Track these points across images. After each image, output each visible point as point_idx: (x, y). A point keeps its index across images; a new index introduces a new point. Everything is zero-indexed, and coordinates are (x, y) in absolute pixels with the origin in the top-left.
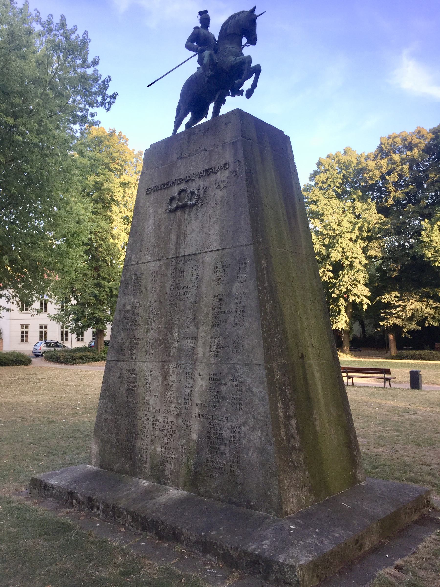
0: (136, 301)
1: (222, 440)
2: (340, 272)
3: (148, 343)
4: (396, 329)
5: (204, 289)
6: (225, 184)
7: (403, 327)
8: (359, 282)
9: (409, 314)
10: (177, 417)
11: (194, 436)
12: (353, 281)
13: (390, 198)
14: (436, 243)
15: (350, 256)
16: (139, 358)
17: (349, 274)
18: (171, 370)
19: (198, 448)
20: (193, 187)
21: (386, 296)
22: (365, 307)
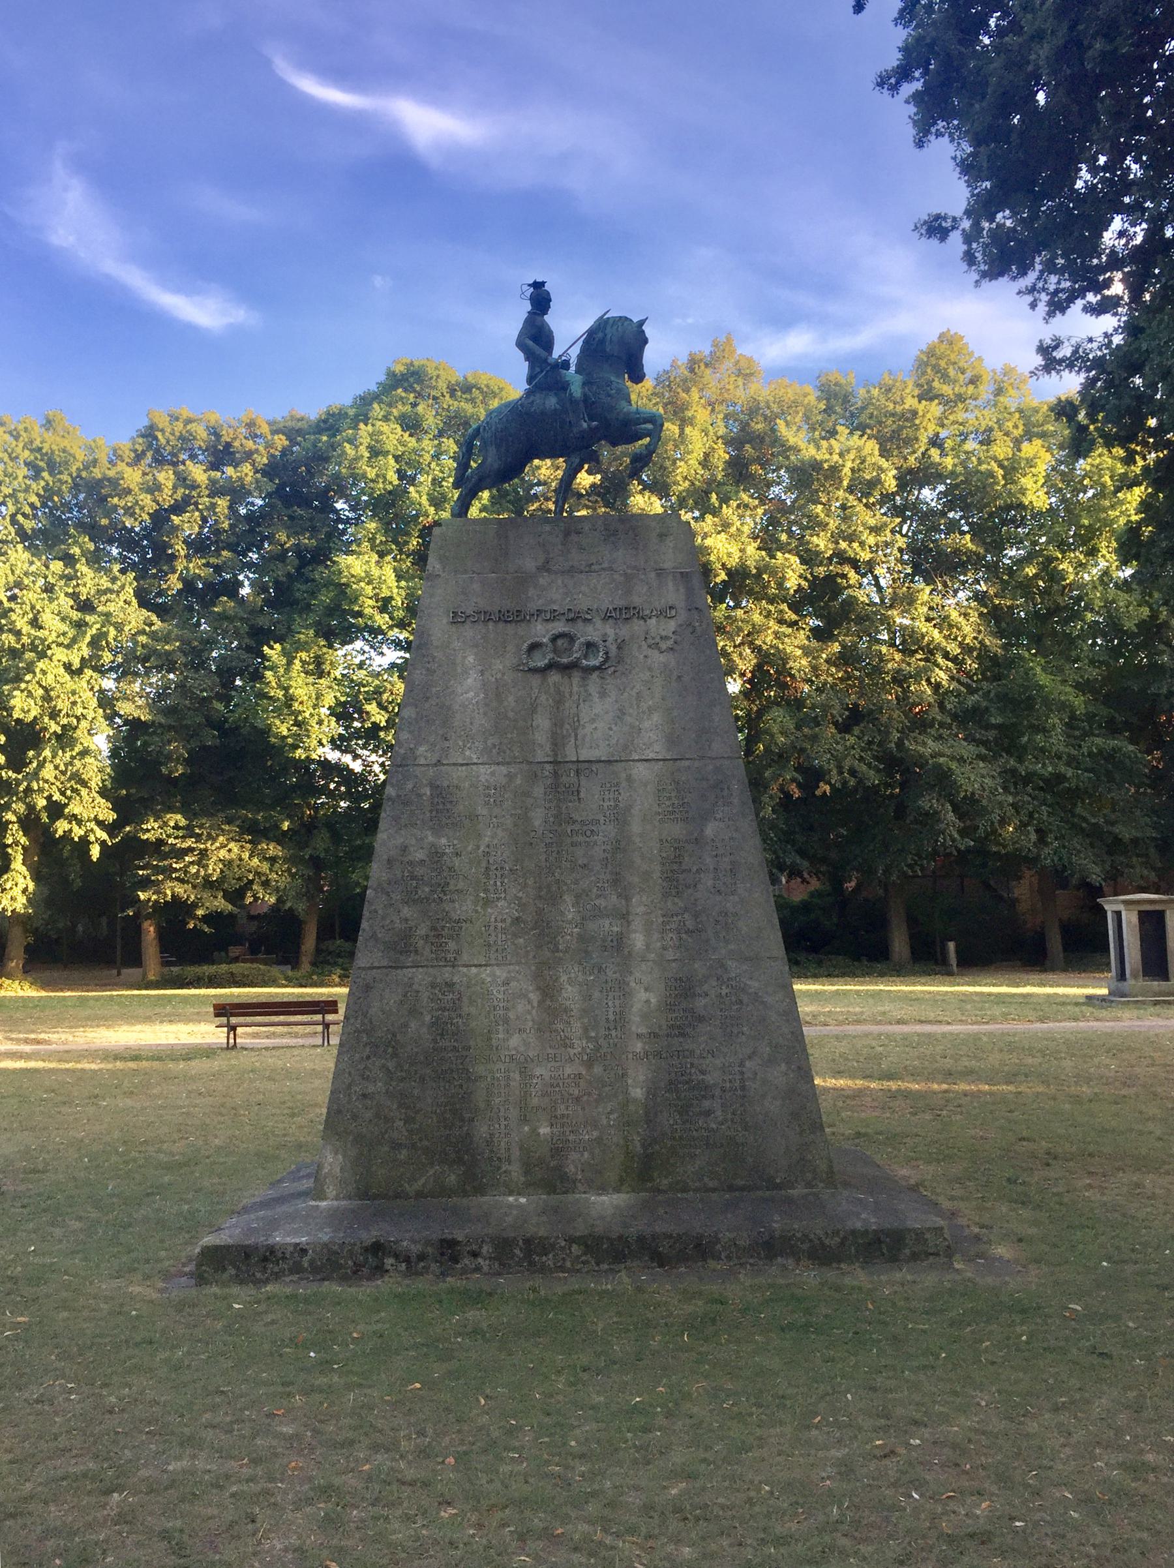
0: (444, 841)
1: (704, 1090)
2: (31, 753)
3: (492, 928)
4: (178, 909)
5: (636, 827)
6: (670, 643)
7: (195, 905)
8: (84, 784)
9: (214, 869)
10: (589, 1064)
11: (638, 1093)
12: (70, 779)
13: (174, 571)
14: (301, 703)
15: (64, 712)
16: (465, 957)
17: (57, 761)
18: (564, 978)
19: (647, 1114)
20: (592, 632)
21: (151, 824)
22: (95, 852)
